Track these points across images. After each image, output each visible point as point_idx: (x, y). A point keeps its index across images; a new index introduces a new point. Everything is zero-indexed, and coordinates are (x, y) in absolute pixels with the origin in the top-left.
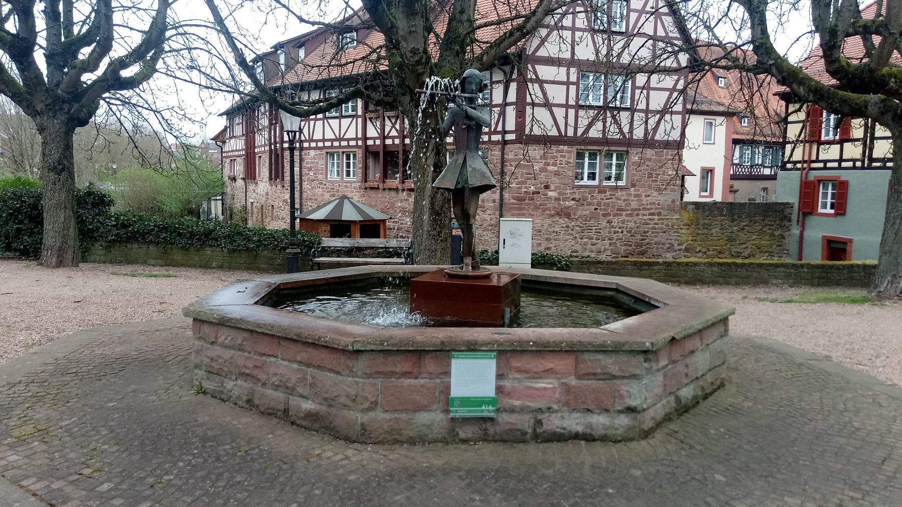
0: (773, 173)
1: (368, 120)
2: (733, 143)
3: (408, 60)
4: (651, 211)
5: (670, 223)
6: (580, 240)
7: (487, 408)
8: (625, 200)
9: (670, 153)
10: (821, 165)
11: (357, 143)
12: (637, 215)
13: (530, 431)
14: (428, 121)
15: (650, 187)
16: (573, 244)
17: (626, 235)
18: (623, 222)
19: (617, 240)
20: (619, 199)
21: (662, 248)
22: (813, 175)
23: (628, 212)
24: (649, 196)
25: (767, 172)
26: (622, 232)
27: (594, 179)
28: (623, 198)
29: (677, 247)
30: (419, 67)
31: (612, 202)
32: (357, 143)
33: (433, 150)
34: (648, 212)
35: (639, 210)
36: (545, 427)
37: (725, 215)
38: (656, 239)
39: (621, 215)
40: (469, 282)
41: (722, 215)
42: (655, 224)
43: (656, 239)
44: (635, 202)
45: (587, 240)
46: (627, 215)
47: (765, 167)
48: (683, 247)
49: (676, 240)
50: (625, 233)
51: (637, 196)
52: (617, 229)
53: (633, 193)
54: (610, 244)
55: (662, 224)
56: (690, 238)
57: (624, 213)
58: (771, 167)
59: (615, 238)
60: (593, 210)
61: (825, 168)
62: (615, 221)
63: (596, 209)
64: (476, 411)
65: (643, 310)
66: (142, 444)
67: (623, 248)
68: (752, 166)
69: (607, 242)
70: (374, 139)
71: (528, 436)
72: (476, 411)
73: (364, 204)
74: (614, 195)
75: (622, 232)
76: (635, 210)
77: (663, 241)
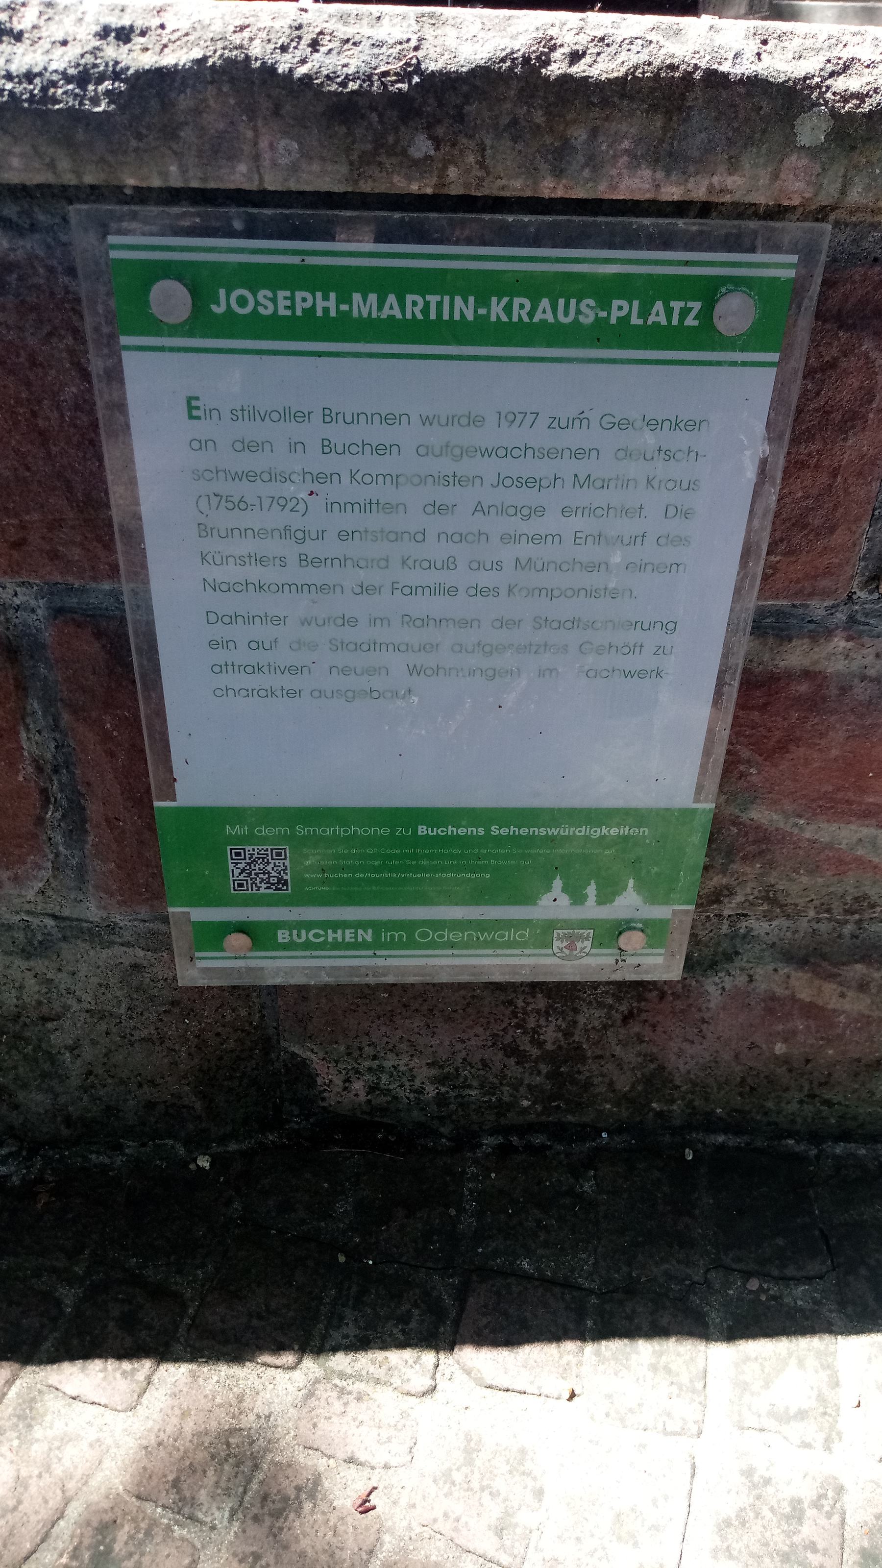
7: (592, 910)
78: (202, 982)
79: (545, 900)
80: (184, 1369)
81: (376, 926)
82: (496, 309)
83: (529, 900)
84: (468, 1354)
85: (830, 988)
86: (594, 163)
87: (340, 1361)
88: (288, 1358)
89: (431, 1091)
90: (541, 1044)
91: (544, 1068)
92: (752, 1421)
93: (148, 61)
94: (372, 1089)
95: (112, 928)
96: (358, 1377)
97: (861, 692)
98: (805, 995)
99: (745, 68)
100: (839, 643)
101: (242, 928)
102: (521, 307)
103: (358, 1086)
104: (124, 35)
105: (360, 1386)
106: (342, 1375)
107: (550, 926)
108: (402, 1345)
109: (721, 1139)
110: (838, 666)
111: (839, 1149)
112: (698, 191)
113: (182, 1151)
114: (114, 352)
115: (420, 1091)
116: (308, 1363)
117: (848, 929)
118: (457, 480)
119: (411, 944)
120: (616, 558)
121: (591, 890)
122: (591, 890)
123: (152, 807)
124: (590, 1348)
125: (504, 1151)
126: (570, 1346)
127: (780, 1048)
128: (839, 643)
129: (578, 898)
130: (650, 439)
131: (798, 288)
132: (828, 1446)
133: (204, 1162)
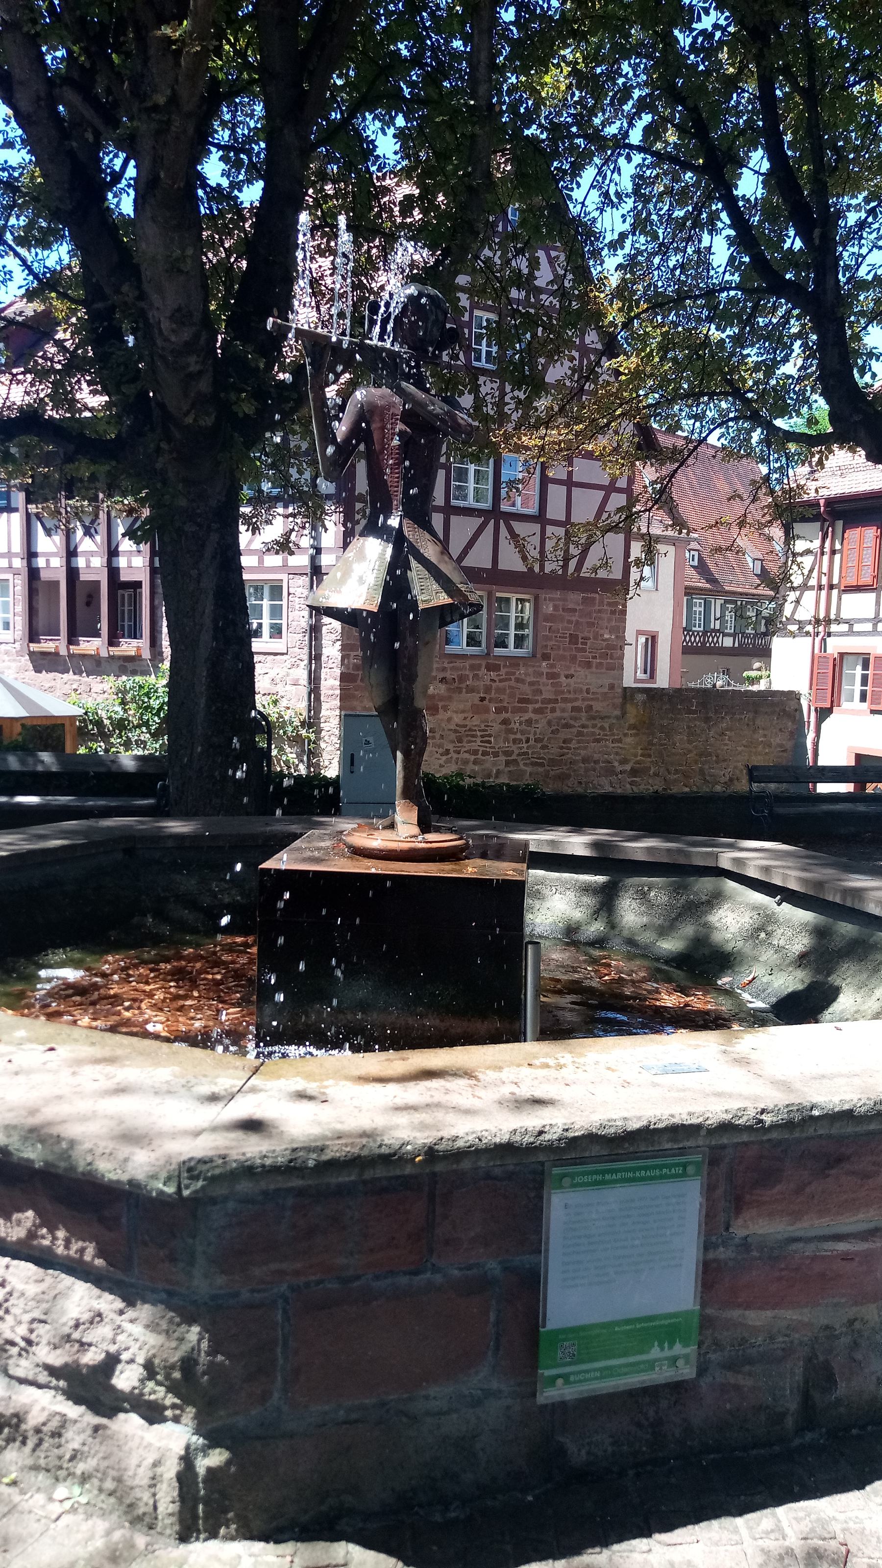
0: (736, 645)
1: (34, 518)
2: (686, 594)
3: (166, 340)
4: (576, 704)
5: (607, 726)
6: (455, 756)
7: (667, 1353)
8: (531, 684)
9: (608, 598)
10: (844, 628)
11: (10, 563)
12: (553, 710)
13: (793, 1406)
14: (867, 52)
15: (573, 659)
16: (442, 762)
17: (534, 747)
18: (529, 722)
19: (519, 755)
20: (522, 681)
21: (594, 770)
22: (835, 646)
23: (537, 706)
24: (572, 676)
25: (728, 642)
26: (528, 741)
27: (478, 644)
28: (529, 679)
29: (619, 768)
30: (192, 359)
31: (510, 687)
32: (10, 563)
33: (214, 557)
34: (569, 705)
35: (556, 701)
36: (842, 1389)
37: (695, 712)
38: (583, 752)
39: (526, 710)
40: (114, 803)
41: (690, 712)
42: (583, 726)
43: (583, 752)
44: (549, 687)
45: (467, 756)
46: (536, 711)
47: (725, 635)
48: (628, 767)
49: (617, 754)
50: (532, 742)
51: (552, 676)
52: (519, 736)
53: (545, 671)
54: (507, 763)
55: (594, 726)
56: (640, 752)
57: (531, 707)
58: (734, 635)
59: (516, 752)
60: (477, 701)
61: (851, 633)
62: (516, 720)
63: (482, 699)
64: (635, 1367)
65: (295, 828)
66: (73, 388)
67: (529, 769)
68: (705, 633)
69: (502, 758)
70: (48, 555)
71: (789, 1422)
72: (635, 1367)
73: (29, 684)
74: (514, 674)
75: (528, 741)
76: (550, 701)
77: (596, 756)
78: (545, 1402)
79: (653, 1351)
80: (563, 1561)
81: (601, 1370)
82: (637, 1174)
83: (648, 1352)
84: (657, 1536)
85: (740, 1376)
86: (659, 1143)
87: (616, 1547)
88: (598, 1549)
89: (610, 1449)
90: (647, 1419)
91: (650, 1430)
92: (758, 1536)
93: (572, 1135)
94: (588, 1453)
95: (500, 1391)
96: (624, 1551)
97: (731, 1264)
98: (732, 1381)
99: (689, 1122)
100: (722, 1249)
101: (559, 1376)
102: (643, 1173)
103: (583, 1452)
104: (567, 1130)
105: (625, 1554)
106: (619, 1552)
107: (656, 1360)
108: (635, 1538)
109: (712, 1456)
110: (722, 1256)
111: (754, 1452)
112: (681, 1146)
113: (520, 1496)
114: (550, 1194)
115: (605, 1451)
116: (605, 1551)
117: (740, 1353)
118: (629, 1216)
119: (612, 1376)
120: (668, 1233)
121: (666, 1345)
122: (666, 1345)
123: (538, 1331)
124: (696, 1527)
125: (638, 1475)
126: (690, 1527)
127: (728, 1406)
128: (722, 1249)
129: (662, 1349)
130: (674, 1200)
131: (703, 1162)
132: (784, 1539)
133: (530, 1498)
